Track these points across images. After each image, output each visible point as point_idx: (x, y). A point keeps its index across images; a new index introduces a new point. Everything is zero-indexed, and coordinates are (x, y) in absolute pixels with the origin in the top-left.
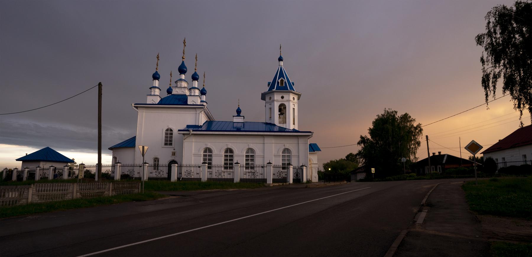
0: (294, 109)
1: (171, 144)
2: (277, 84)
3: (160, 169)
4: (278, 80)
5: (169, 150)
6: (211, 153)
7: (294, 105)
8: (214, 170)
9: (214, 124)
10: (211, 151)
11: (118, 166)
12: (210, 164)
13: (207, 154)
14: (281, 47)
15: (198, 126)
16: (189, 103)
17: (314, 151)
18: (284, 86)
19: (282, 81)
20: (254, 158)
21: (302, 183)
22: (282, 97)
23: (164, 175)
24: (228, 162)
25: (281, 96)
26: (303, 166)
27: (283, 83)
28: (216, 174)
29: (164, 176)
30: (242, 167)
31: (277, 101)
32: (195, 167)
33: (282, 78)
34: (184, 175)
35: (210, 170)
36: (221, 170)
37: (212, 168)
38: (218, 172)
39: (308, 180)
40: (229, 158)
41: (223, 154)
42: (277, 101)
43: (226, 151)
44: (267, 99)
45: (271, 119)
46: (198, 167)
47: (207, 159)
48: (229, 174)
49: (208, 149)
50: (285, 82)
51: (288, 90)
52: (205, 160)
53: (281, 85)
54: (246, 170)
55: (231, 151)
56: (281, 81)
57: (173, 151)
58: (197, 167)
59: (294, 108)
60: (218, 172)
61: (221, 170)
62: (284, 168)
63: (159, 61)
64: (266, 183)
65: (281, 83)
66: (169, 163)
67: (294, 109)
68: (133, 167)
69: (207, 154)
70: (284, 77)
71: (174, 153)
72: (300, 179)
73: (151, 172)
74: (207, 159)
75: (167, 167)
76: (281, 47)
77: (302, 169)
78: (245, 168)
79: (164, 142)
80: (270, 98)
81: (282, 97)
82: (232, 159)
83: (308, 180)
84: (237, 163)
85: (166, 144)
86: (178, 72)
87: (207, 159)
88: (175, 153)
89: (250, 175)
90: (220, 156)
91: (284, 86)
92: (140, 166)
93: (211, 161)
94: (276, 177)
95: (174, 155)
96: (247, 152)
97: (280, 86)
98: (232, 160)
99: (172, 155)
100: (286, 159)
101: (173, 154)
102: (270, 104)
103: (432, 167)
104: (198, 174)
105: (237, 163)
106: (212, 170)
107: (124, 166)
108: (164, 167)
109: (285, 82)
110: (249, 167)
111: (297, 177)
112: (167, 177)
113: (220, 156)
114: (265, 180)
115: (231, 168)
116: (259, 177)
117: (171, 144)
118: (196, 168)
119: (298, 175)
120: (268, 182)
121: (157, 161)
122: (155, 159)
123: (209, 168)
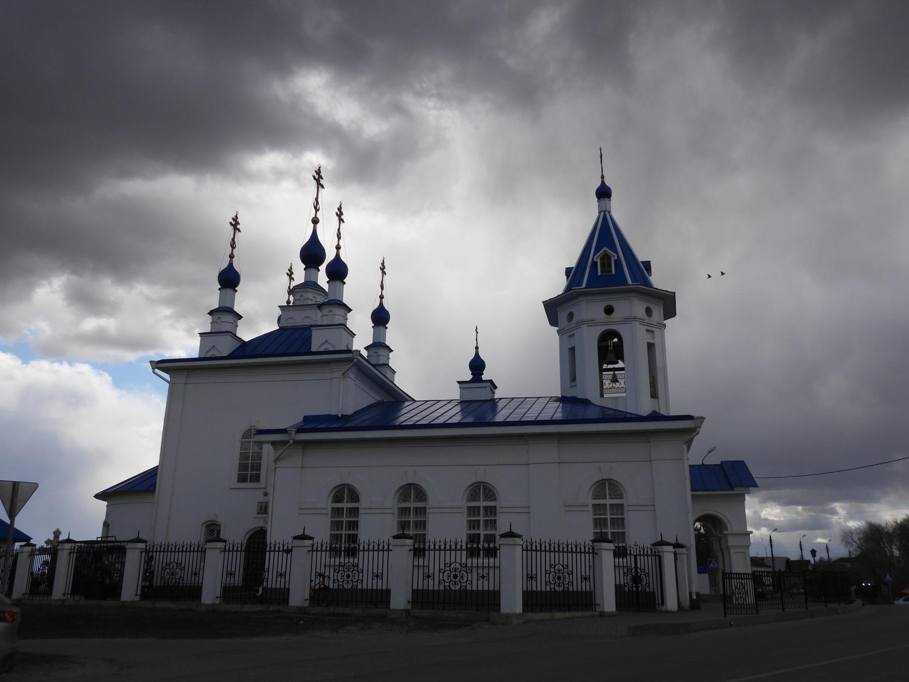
0: (653, 344)
1: (256, 479)
2: (591, 268)
3: (561, 563)
4: (594, 255)
5: (251, 496)
6: (495, 500)
7: (652, 332)
8: (435, 561)
9: (407, 407)
10: (494, 494)
11: (66, 552)
12: (421, 538)
13: (345, 505)
14: (601, 156)
15: (337, 416)
16: (314, 349)
17: (732, 489)
18: (613, 273)
19: (606, 258)
20: (622, 514)
21: (661, 611)
22: (609, 311)
23: (185, 579)
24: (482, 532)
25: (602, 306)
26: (662, 543)
27: (610, 265)
28: (470, 578)
29: (185, 582)
30: (383, 550)
31: (592, 323)
32: (456, 550)
33: (605, 248)
34: (159, 577)
35: (492, 560)
36: (458, 560)
37: (427, 552)
38: (552, 570)
39: (694, 597)
40: (482, 518)
41: (463, 503)
42: (592, 323)
43: (338, 497)
44: (562, 316)
45: (574, 384)
46: (283, 551)
47: (479, 521)
48: (483, 577)
49: (485, 489)
50: (618, 262)
51: (627, 285)
52: (403, 525)
53: (602, 272)
54: (469, 561)
55: (421, 494)
56: (602, 259)
57: (262, 498)
58: (279, 551)
59: (651, 341)
60: (552, 570)
61: (458, 560)
62: (473, 553)
63: (238, 234)
64: (288, 603)
65: (603, 265)
66: (247, 537)
67: (653, 344)
68: (184, 553)
69: (345, 505)
70: (615, 247)
71: (264, 505)
72: (652, 594)
73: (375, 571)
74: (481, 522)
75: (243, 553)
76: (601, 156)
77: (660, 557)
78: (464, 553)
79: (235, 472)
80: (571, 316)
81: (609, 311)
82: (425, 522)
83: (694, 597)
84: (511, 535)
85: (242, 479)
86: (595, 196)
87: (479, 521)
88: (266, 507)
89: (465, 574)
90: (316, 511)
91: (613, 273)
92: (285, 548)
93: (357, 529)
94: (540, 586)
95: (266, 512)
96: (472, 495)
97: (599, 273)
98: (493, 524)
99: (258, 513)
100: (482, 518)
101: (261, 509)
102: (570, 336)
103: (854, 543)
104: (281, 575)
105: (511, 535)
106: (356, 560)
107: (233, 551)
108: (373, 550)
109: (615, 261)
110: (478, 549)
111: (637, 587)
112: (240, 584)
113: (316, 511)
114: (383, 596)
115: (492, 552)
116: (368, 583)
117: (256, 479)
118: (277, 553)
119: (641, 580)
120: (504, 609)
121: (215, 533)
122: (210, 525)
123: (419, 552)
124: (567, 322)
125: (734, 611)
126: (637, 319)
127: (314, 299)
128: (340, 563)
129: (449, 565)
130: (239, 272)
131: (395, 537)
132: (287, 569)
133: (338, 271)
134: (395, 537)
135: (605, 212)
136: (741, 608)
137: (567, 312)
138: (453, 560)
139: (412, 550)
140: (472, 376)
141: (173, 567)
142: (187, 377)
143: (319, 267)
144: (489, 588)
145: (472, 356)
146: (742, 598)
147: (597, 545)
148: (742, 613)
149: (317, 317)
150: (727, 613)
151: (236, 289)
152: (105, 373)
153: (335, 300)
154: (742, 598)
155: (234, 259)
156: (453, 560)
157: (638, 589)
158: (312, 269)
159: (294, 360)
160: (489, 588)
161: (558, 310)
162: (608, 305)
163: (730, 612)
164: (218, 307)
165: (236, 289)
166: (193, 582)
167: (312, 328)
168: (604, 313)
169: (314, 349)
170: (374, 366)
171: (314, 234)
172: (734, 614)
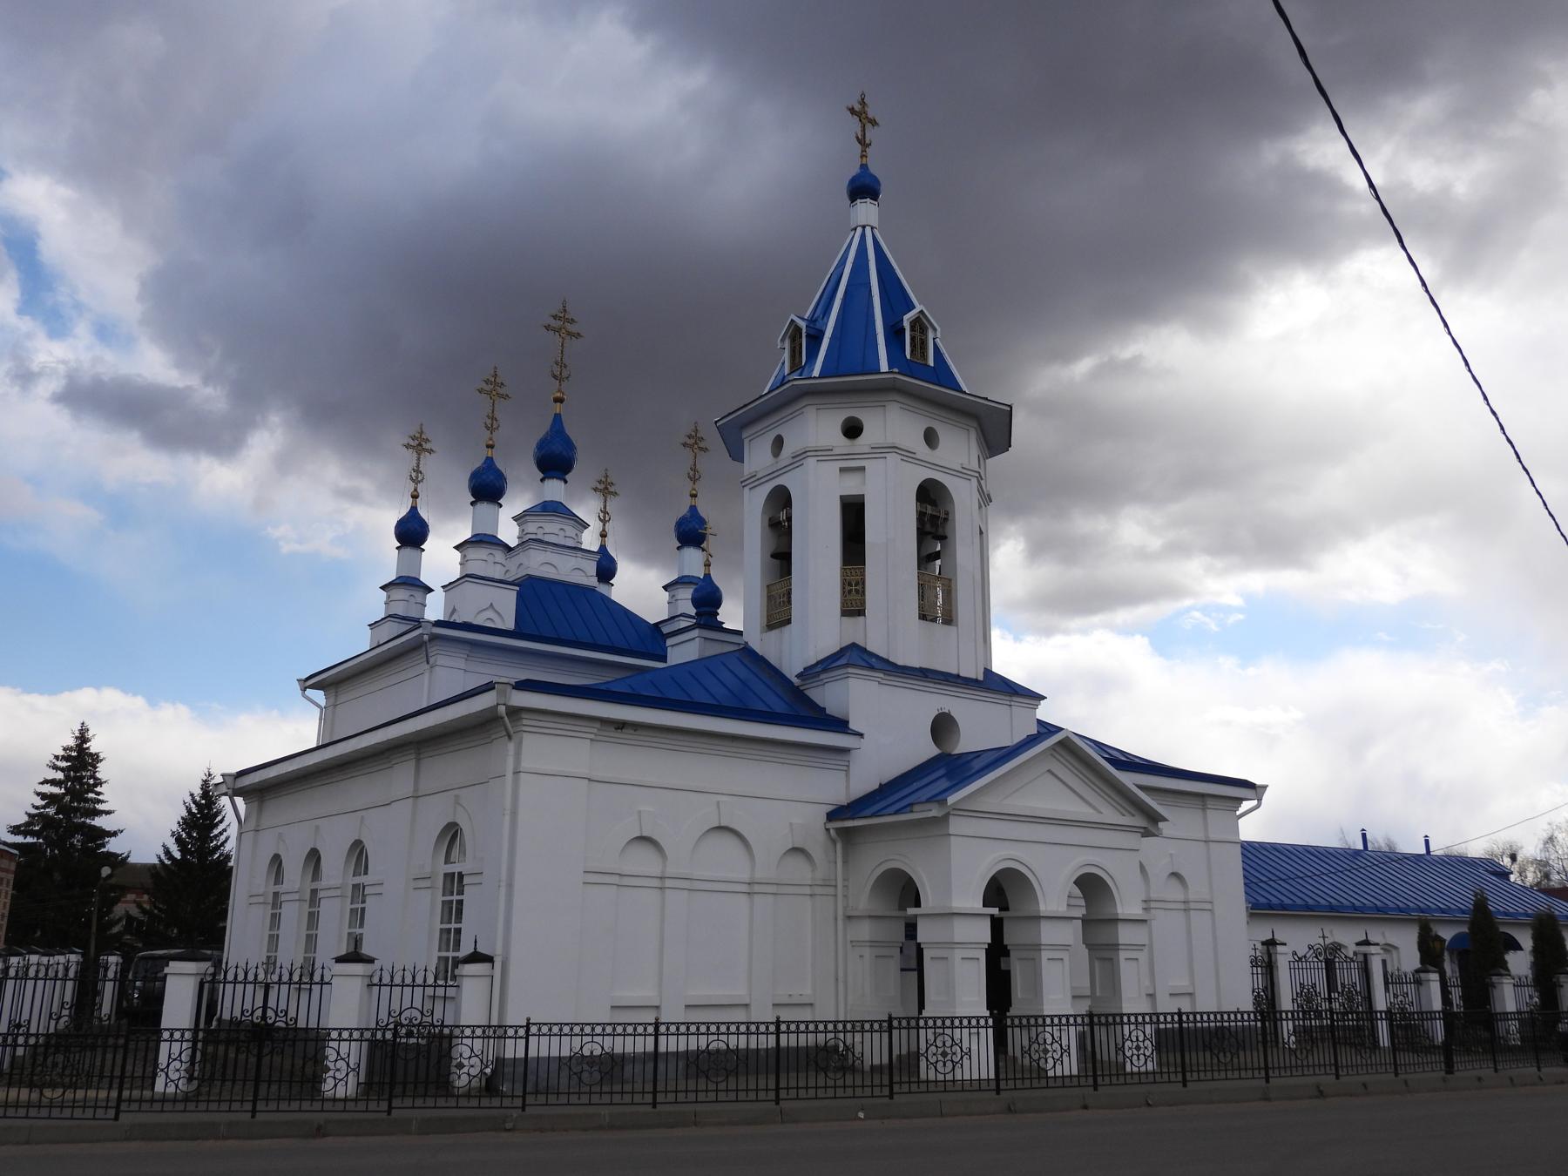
22: (852, 430)
33: (906, 317)
75: (990, 1031)
81: (852, 430)
112: (1075, 1072)
124: (772, 457)
126: (809, 454)
127: (562, 533)
129: (250, 1012)
131: (339, 960)
134: (339, 960)
135: (864, 227)
136: (1325, 1065)
137: (771, 436)
138: (406, 1004)
139: (1154, 1004)
141: (1302, 1053)
142: (336, 696)
147: (1423, 975)
150: (1399, 1072)
152: (1559, 886)
156: (406, 1004)
157: (197, 1036)
159: (578, 654)
161: (744, 436)
162: (849, 418)
163: (1404, 1071)
166: (545, 1084)
168: (841, 435)
172: (1308, 1075)
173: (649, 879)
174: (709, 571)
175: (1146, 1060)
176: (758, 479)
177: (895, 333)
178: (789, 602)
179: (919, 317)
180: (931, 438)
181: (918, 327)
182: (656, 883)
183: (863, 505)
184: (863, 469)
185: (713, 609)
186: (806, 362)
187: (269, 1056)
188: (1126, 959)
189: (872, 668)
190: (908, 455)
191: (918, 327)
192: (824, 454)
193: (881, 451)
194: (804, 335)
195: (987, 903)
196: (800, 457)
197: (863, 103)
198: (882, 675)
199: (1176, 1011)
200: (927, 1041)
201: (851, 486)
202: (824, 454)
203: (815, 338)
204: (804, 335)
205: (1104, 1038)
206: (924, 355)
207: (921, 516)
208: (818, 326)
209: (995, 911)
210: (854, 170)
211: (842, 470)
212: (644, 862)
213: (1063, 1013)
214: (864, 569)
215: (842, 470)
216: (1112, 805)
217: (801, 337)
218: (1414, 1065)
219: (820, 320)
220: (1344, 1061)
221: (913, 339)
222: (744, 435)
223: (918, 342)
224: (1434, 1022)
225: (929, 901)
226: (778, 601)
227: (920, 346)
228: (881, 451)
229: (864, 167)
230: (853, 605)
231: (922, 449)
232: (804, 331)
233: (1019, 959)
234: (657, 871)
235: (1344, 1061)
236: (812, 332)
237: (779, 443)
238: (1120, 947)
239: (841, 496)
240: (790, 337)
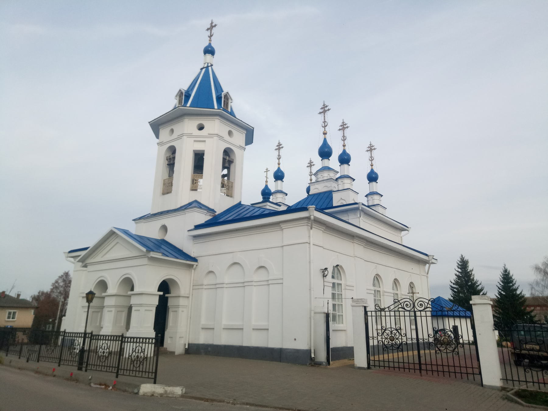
125: (71, 363)
126: (184, 135)
127: (329, 176)
128: (382, 327)
130: (283, 171)
132: (126, 363)
133: (345, 159)
140: (262, 199)
143: (330, 158)
144: (455, 324)
145: (263, 187)
146: (103, 348)
148: (68, 365)
149: (333, 186)
151: (283, 180)
153: (344, 175)
154: (103, 348)
155: (280, 165)
158: (325, 159)
160: (455, 324)
164: (369, 192)
165: (283, 180)
167: (333, 193)
169: (334, 205)
170: (368, 207)
171: (325, 140)
173: (248, 283)
174: (266, 183)
175: (135, 350)
176: (163, 143)
177: (219, 99)
178: (172, 185)
179: (226, 94)
180: (230, 133)
181: (226, 98)
182: (266, 283)
183: (203, 154)
184: (205, 141)
185: (268, 196)
186: (184, 105)
187: (137, 346)
188: (108, 311)
189: (201, 208)
190: (221, 137)
191: (226, 98)
192: (190, 135)
193: (211, 135)
194: (184, 95)
195: (159, 290)
196: (180, 137)
197: (215, 25)
198: (206, 212)
199: (121, 334)
200: (433, 329)
201: (199, 147)
202: (190, 135)
203: (188, 96)
204: (184, 95)
205: (37, 349)
206: (227, 107)
207: (224, 159)
208: (190, 93)
209: (161, 293)
210: (207, 44)
211: (195, 141)
212: (262, 276)
213: (115, 334)
214: (203, 175)
215: (195, 141)
216: (102, 251)
217: (182, 96)
218: (69, 361)
219: (190, 91)
220: (64, 358)
221: (224, 101)
222: (160, 128)
223: (226, 103)
224: (97, 341)
225: (137, 290)
226: (167, 185)
227: (226, 104)
228: (211, 135)
229: (210, 44)
230: (194, 187)
231: (227, 137)
232: (184, 93)
233: (172, 311)
234: (266, 279)
235: (64, 358)
236: (187, 94)
237: (172, 131)
238: (180, 306)
239: (194, 151)
240: (179, 96)
